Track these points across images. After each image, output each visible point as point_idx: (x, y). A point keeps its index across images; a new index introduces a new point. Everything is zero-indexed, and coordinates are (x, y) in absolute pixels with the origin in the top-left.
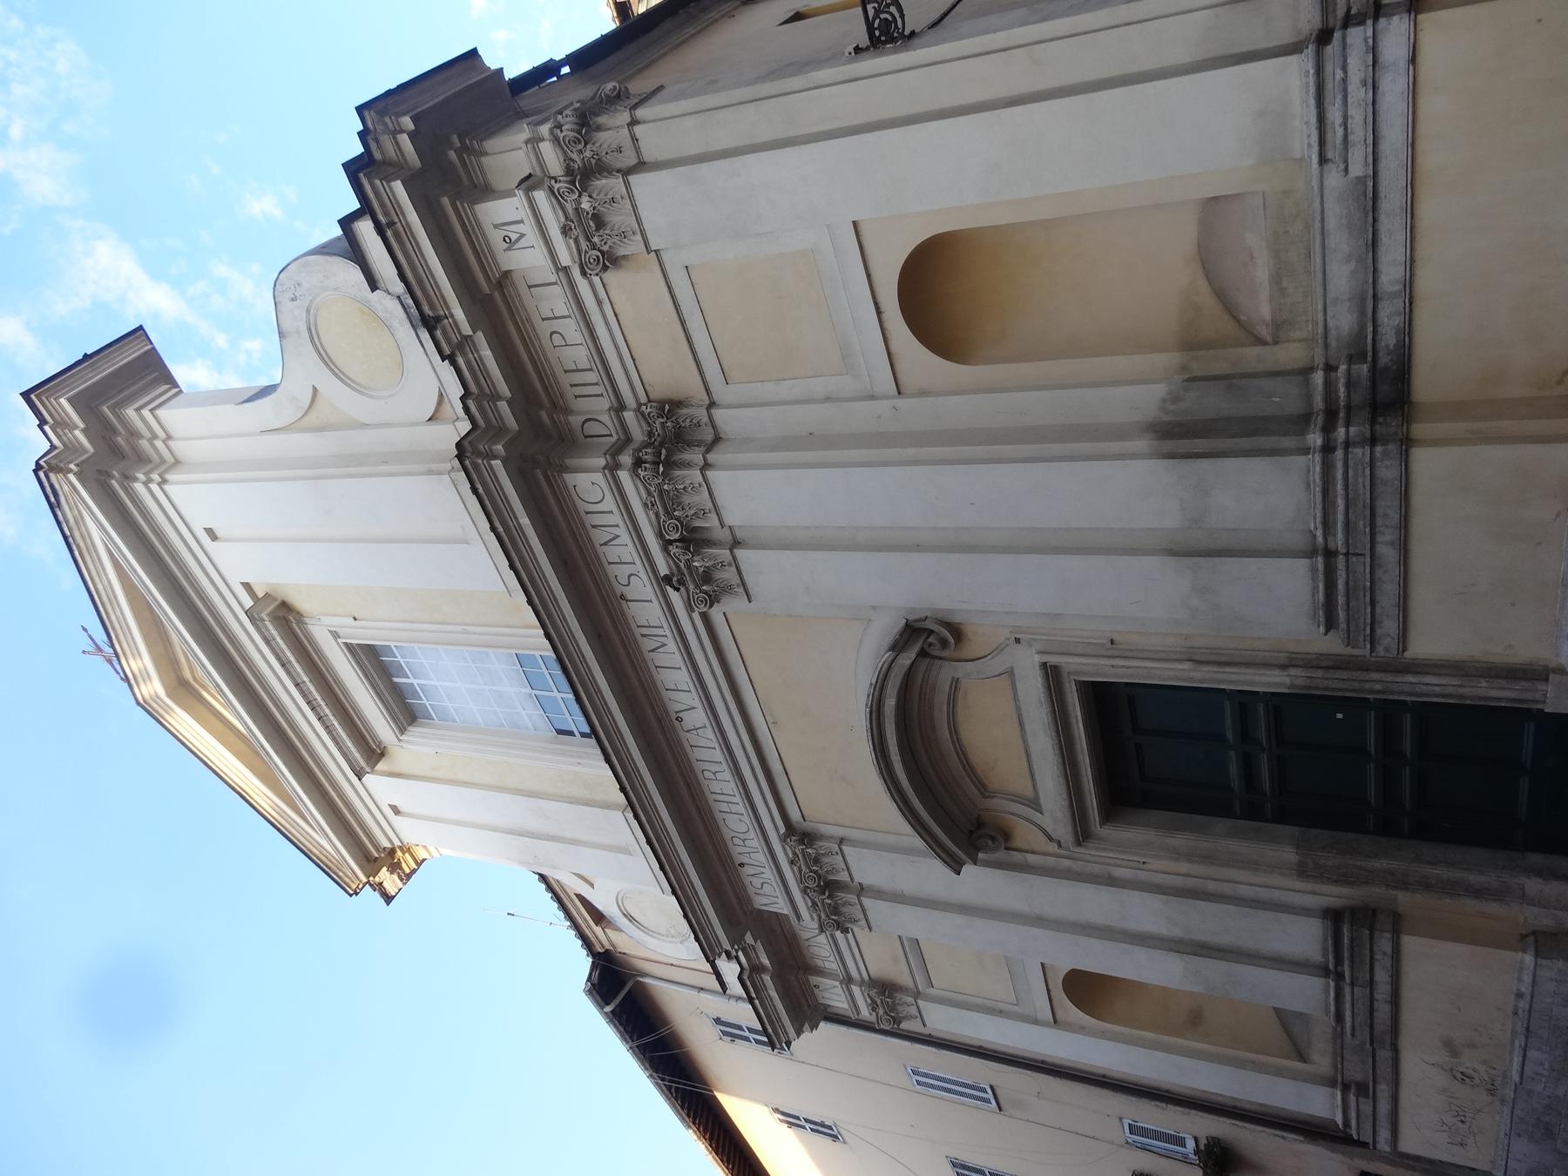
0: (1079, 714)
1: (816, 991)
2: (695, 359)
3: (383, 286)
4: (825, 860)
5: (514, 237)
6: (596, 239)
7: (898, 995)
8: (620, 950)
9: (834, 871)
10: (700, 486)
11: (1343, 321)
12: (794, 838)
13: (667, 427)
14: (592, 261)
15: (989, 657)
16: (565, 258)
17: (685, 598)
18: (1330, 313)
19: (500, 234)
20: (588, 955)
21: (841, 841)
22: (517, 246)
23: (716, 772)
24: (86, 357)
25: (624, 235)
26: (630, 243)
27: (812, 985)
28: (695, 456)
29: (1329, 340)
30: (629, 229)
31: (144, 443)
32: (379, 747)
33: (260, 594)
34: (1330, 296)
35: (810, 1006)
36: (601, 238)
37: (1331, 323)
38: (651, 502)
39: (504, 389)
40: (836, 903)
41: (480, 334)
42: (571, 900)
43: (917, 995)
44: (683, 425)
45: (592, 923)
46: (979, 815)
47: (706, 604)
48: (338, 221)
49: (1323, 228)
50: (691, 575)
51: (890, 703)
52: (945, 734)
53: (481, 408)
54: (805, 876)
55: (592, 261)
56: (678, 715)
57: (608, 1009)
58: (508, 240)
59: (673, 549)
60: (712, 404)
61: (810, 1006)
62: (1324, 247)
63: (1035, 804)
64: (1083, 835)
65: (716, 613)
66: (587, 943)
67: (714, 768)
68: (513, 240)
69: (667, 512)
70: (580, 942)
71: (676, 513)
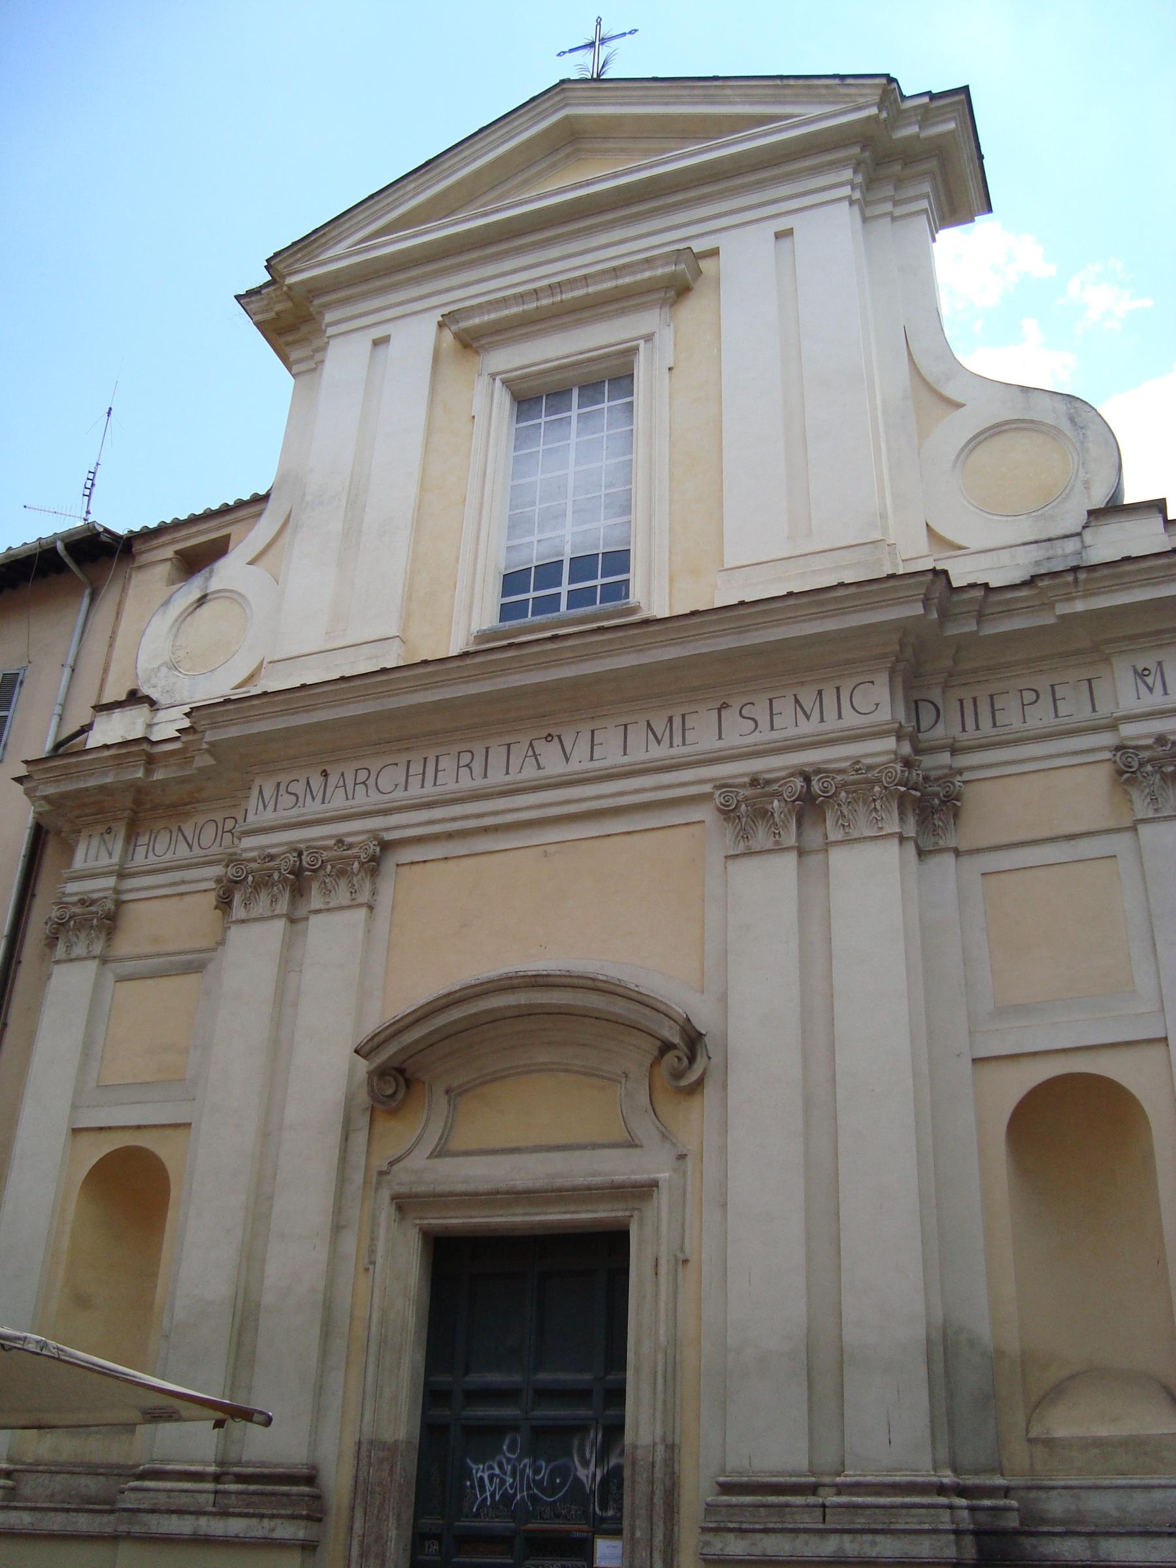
0: (583, 1216)
1: (102, 828)
2: (1011, 845)
3: (1093, 524)
4: (343, 883)
5: (1149, 680)
6: (1149, 768)
7: (103, 936)
8: (134, 575)
9: (327, 891)
10: (881, 828)
11: (1056, 1506)
12: (378, 849)
13: (933, 799)
14: (1129, 759)
15: (657, 1122)
16: (1128, 730)
17: (730, 781)
18: (1064, 1492)
19: (1153, 667)
20: (131, 532)
21: (371, 908)
22: (1139, 681)
23: (471, 769)
24: (981, 157)
25: (1154, 800)
26: (1145, 804)
27: (113, 825)
28: (911, 830)
29: (1035, 1491)
30: (1160, 805)
31: (889, 191)
32: (482, 346)
33: (704, 264)
34: (1083, 1493)
35: (78, 817)
36: (1150, 774)
37: (1054, 1493)
38: (860, 769)
39: (989, 630)
40: (273, 885)
41: (1051, 621)
42: (219, 528)
43: (104, 960)
44: (935, 816)
45: (179, 547)
46: (424, 1083)
47: (724, 805)
48: (1164, 499)
49: (1154, 1487)
50: (765, 795)
51: (596, 1001)
52: (542, 1057)
53: (971, 601)
54: (316, 853)
55: (1129, 759)
56: (556, 739)
57: (60, 546)
58: (1146, 673)
59: (799, 783)
60: (957, 853)
61: (78, 817)
62: (1133, 1487)
63: (440, 1152)
64: (403, 1204)
65: (705, 814)
66: (147, 534)
67: (478, 766)
68: (1145, 678)
69: (844, 785)
70: (153, 524)
71: (843, 794)
